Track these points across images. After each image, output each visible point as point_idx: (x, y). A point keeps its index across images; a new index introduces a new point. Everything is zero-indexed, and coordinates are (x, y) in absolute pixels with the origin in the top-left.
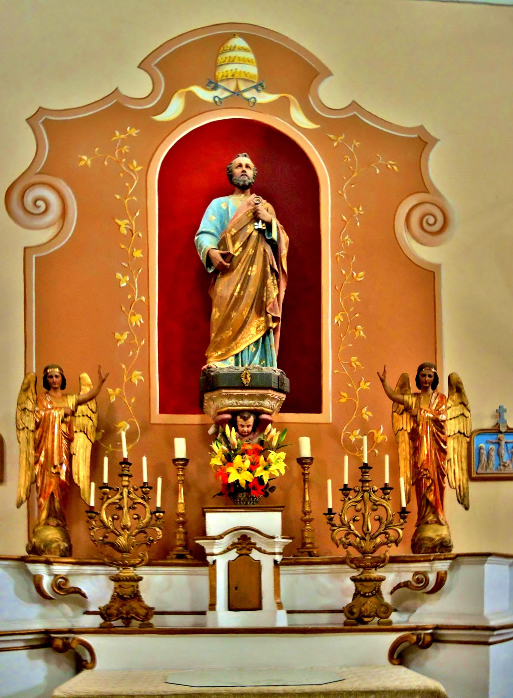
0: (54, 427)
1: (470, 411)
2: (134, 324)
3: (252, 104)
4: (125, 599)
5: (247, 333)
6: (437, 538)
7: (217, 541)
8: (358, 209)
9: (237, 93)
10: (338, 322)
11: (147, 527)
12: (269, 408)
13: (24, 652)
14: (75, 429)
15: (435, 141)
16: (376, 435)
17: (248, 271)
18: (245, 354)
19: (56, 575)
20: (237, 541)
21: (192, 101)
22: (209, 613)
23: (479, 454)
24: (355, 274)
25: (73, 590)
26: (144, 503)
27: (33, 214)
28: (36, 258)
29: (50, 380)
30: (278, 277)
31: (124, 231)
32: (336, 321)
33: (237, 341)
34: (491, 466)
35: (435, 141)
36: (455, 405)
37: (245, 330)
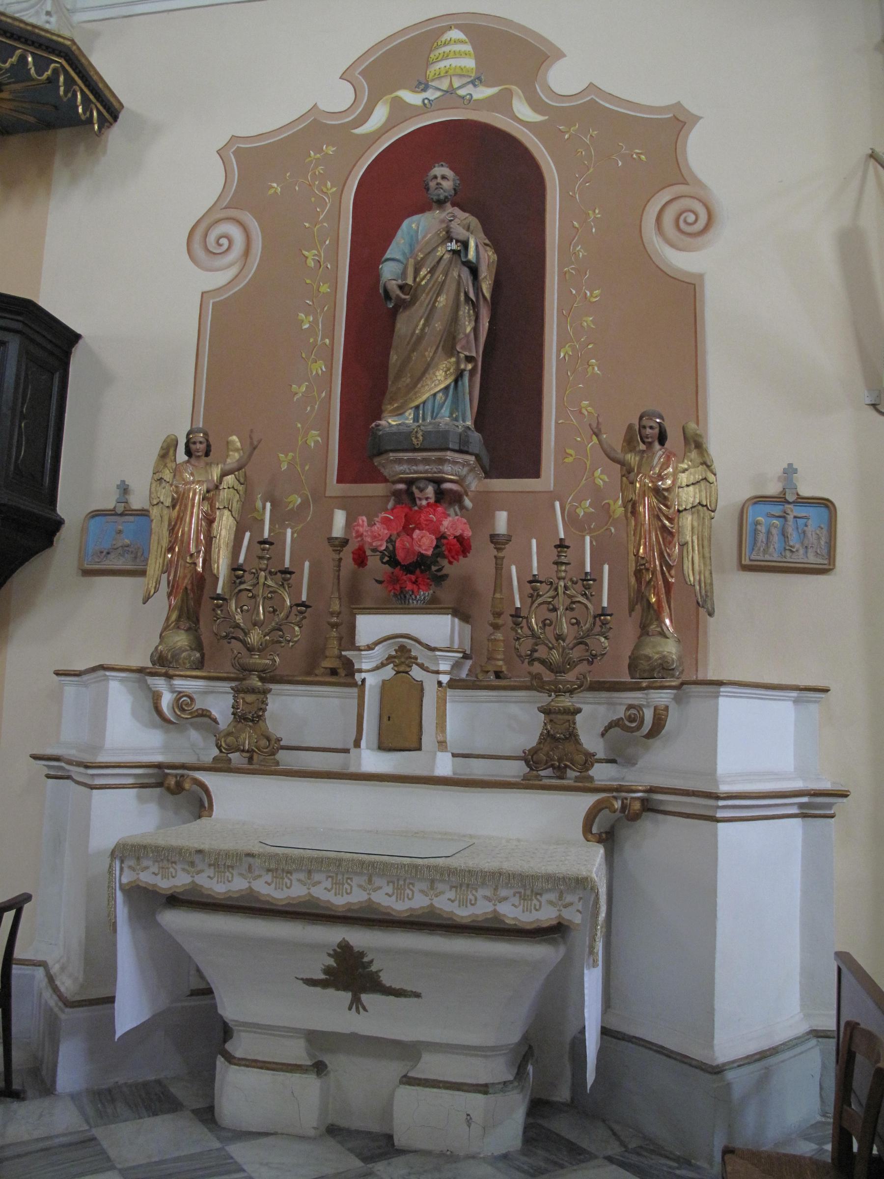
0: (193, 506)
1: (715, 475)
2: (314, 373)
3: (467, 101)
4: (557, 740)
5: (431, 378)
6: (657, 656)
7: (363, 653)
8: (594, 211)
9: (451, 91)
10: (564, 357)
11: (588, 636)
12: (452, 475)
13: (134, 791)
14: (217, 506)
15: (696, 119)
16: (612, 508)
17: (436, 300)
18: (429, 406)
19: (180, 692)
20: (394, 653)
21: (398, 105)
22: (353, 751)
23: (756, 532)
24: (588, 294)
25: (200, 712)
26: (585, 601)
27: (214, 253)
28: (213, 303)
29: (193, 447)
30: (475, 306)
31: (311, 263)
32: (562, 355)
33: (417, 389)
34: (771, 549)
35: (696, 119)
36: (694, 467)
37: (427, 376)
